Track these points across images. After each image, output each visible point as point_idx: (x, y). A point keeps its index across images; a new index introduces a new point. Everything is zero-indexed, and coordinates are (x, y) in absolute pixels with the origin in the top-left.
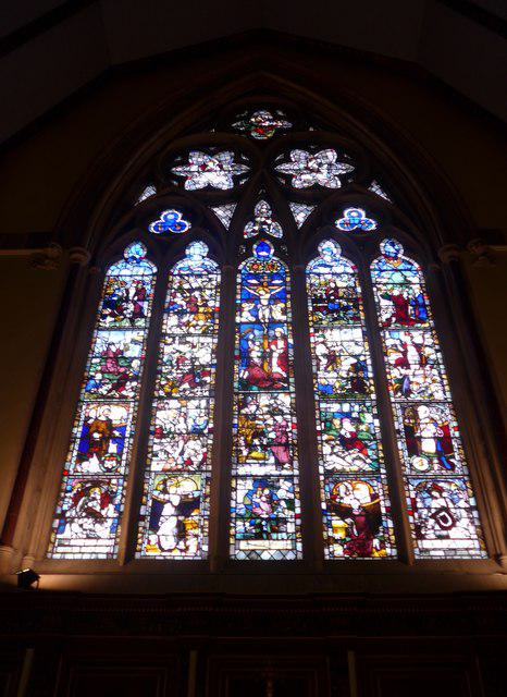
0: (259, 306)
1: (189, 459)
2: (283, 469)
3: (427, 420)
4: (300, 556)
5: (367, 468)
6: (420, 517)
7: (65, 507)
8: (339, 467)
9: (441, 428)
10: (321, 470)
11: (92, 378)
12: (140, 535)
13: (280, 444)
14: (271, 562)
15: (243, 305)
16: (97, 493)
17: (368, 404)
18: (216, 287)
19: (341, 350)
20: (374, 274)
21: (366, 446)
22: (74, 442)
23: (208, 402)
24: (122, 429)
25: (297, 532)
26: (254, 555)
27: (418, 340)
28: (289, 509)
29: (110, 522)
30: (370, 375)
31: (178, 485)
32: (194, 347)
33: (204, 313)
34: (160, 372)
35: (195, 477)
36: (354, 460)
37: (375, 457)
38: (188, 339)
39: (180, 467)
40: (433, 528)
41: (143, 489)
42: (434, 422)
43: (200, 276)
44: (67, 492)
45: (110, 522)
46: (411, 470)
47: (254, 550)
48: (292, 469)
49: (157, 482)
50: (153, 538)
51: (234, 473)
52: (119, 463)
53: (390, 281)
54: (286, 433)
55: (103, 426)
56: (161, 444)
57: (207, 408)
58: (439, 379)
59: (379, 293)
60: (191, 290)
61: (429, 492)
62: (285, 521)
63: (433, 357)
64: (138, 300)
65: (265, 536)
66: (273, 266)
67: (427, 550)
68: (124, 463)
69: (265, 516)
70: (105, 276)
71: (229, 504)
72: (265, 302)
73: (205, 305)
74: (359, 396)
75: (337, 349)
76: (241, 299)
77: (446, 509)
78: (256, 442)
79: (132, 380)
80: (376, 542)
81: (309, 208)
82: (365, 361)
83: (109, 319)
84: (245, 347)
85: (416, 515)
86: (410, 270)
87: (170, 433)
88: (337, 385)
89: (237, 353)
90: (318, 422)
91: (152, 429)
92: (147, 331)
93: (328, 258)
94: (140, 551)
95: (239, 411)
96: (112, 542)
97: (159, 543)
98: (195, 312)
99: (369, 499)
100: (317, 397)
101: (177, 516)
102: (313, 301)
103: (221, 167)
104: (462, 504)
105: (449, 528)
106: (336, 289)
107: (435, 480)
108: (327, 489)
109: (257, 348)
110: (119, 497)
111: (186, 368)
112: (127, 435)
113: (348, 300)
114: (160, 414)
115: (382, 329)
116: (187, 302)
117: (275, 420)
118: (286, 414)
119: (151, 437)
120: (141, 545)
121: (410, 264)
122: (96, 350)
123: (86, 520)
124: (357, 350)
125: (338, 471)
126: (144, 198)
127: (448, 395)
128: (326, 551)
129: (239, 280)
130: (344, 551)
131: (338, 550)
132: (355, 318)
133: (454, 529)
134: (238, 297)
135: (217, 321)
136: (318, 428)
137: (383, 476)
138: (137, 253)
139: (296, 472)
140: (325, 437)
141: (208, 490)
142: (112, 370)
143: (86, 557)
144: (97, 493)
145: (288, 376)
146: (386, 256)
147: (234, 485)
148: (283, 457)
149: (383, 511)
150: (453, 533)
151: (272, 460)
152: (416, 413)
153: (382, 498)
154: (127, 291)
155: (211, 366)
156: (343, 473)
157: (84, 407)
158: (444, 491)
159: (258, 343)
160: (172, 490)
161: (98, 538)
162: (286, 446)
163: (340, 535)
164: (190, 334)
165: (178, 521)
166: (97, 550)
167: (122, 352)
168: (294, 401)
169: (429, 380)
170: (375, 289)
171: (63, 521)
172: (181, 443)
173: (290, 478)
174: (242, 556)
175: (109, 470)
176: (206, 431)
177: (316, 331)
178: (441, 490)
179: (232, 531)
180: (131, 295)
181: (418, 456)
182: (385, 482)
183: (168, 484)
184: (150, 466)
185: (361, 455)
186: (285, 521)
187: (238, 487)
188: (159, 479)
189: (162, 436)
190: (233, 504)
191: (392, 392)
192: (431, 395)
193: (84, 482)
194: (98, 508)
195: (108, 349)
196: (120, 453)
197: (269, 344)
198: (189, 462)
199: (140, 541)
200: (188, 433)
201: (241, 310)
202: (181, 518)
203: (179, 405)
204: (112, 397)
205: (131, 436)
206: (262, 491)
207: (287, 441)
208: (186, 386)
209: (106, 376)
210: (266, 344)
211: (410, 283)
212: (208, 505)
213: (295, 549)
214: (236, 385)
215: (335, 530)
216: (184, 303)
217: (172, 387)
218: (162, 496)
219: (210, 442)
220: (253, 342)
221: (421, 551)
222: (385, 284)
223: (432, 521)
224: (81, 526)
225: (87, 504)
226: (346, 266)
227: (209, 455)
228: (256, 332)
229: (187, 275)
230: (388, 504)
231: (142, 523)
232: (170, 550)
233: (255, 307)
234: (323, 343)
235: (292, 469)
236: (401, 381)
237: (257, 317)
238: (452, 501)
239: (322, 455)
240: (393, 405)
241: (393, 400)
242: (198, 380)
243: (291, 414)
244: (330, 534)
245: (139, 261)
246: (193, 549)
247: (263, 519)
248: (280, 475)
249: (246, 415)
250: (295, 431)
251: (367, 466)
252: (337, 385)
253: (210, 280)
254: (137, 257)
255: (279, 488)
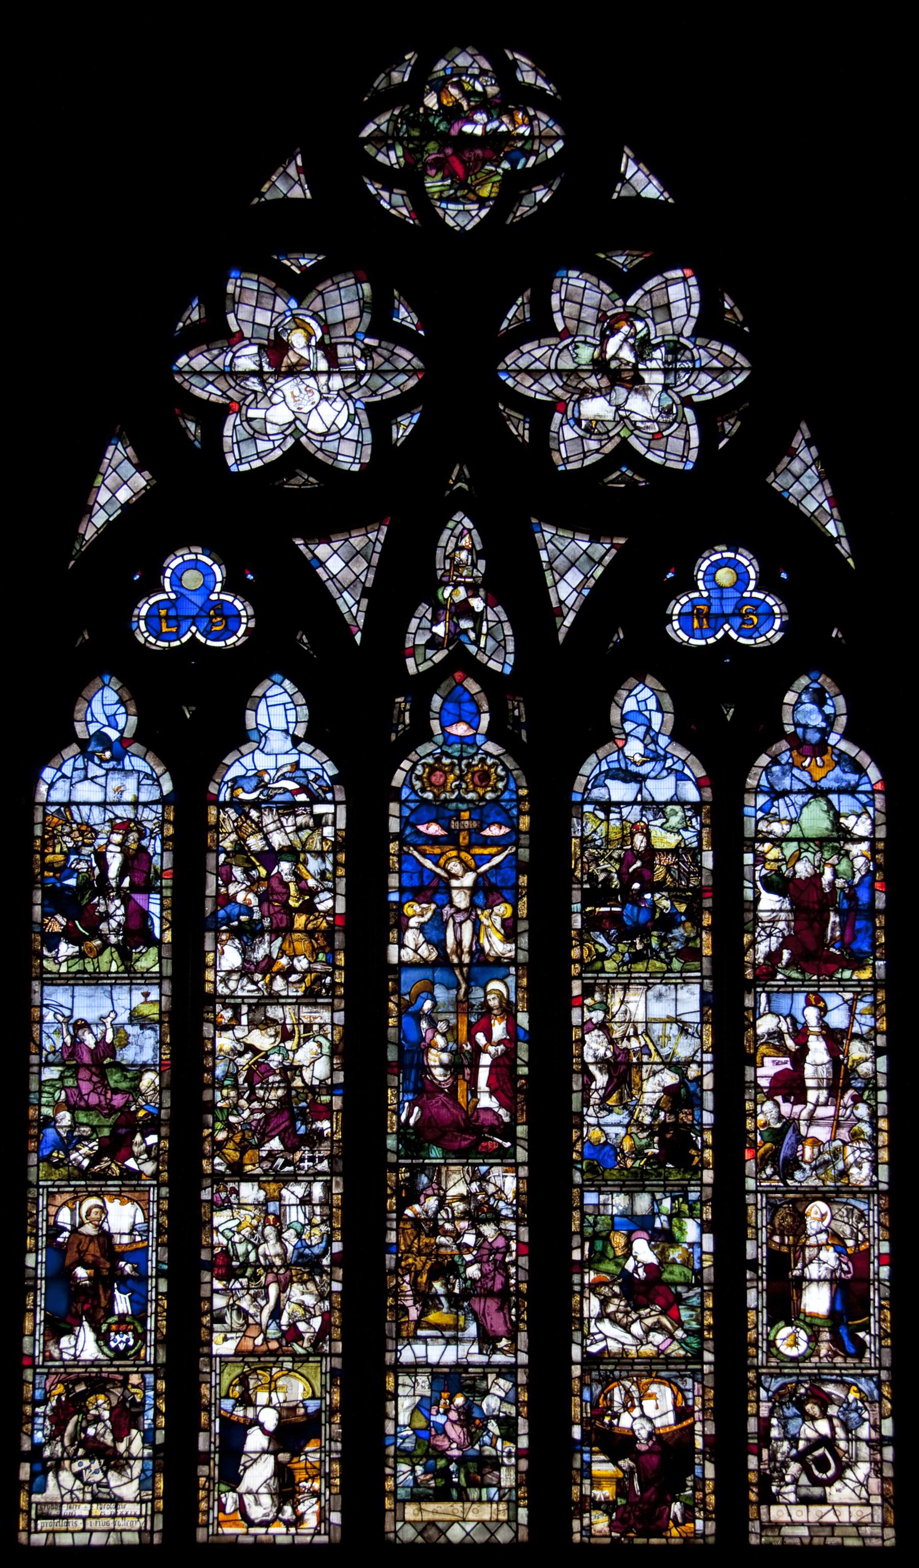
0: (447, 910)
1: (293, 1326)
2: (495, 1350)
3: (823, 1237)
4: (523, 1534)
5: (675, 1349)
6: (773, 1458)
7: (39, 1436)
8: (614, 1347)
9: (850, 1257)
10: (576, 1353)
11: (49, 1122)
12: (202, 1494)
13: (489, 1294)
14: (466, 1548)
15: (408, 910)
16: (101, 1405)
17: (693, 1196)
18: (336, 848)
19: (644, 1050)
20: (755, 803)
21: (679, 1300)
22: (35, 1289)
23: (327, 1188)
24: (137, 1254)
25: (518, 1486)
26: (432, 1532)
27: (837, 1019)
28: (505, 1437)
29: (137, 1467)
30: (708, 1118)
31: (272, 1387)
32: (287, 1036)
33: (310, 934)
34: (212, 1107)
35: (310, 1369)
36: (648, 1331)
37: (694, 1325)
38: (275, 1012)
39: (274, 1345)
40: (795, 1481)
41: (200, 1396)
42: (836, 1240)
43: (290, 808)
44: (36, 1403)
45: (137, 1467)
46: (769, 1354)
47: (432, 1523)
48: (515, 1352)
49: (226, 1380)
50: (230, 1501)
51: (389, 1358)
52: (140, 1337)
53: (795, 831)
54: (505, 1266)
55: (94, 1249)
56: (226, 1291)
57: (326, 1203)
58: (866, 1129)
59: (761, 872)
60: (271, 857)
61: (800, 1405)
62: (495, 1464)
63: (865, 1068)
64: (133, 887)
65: (454, 1493)
66: (485, 777)
67: (778, 1526)
68: (151, 1337)
69: (456, 1453)
70: (31, 804)
71: (382, 1427)
72: (461, 900)
73: (309, 908)
74: (675, 1177)
75: (634, 1044)
76: (401, 890)
77: (828, 1442)
78: (438, 1286)
79: (146, 1129)
80: (676, 1508)
81: (598, 550)
82: (699, 1079)
83: (65, 949)
84: (413, 1036)
85: (765, 1453)
86: (851, 791)
87: (245, 1264)
88: (627, 1145)
89: (392, 1054)
90: (576, 1241)
91: (205, 1255)
92: (167, 987)
93: (634, 748)
94: (206, 1525)
95: (400, 1211)
96: (147, 1509)
97: (241, 1508)
98: (283, 930)
99: (670, 1418)
100: (577, 1178)
101: (275, 1453)
102: (592, 897)
103: (329, 350)
104: (864, 1431)
105: (830, 1482)
106: (651, 852)
107: (817, 1379)
108: (586, 1395)
109: (440, 1041)
110: (150, 1414)
111: (273, 1095)
112: (151, 1272)
113: (675, 895)
114: (220, 1219)
115: (750, 986)
116: (263, 899)
117: (479, 1235)
118: (506, 1218)
119: (206, 1276)
120: (207, 1512)
121: (859, 770)
122: (47, 1044)
123: (86, 1463)
124: (684, 1048)
125: (612, 1356)
126: (90, 533)
127: (884, 1173)
128: (576, 1524)
129: (394, 826)
130: (611, 1525)
131: (600, 1523)
132: (690, 953)
133: (838, 1485)
134: (393, 881)
135: (341, 959)
136: (576, 1255)
137: (707, 1369)
138: (112, 721)
139: (523, 1358)
140: (590, 1277)
141: (337, 1397)
142: (94, 1099)
143: (98, 1539)
144: (101, 1405)
145: (514, 1123)
146: (797, 743)
147: (390, 1387)
148: (497, 1323)
149: (699, 1443)
150: (836, 1493)
151: (472, 1330)
152: (800, 1218)
153: (698, 1416)
154: (101, 857)
155: (331, 1089)
156: (622, 1359)
157: (42, 1201)
158: (832, 1402)
159: (442, 1026)
160: (262, 1397)
161: (117, 1501)
162: (503, 1296)
163: (605, 1492)
164: (274, 999)
165: (277, 1463)
166: (121, 1524)
167: (111, 1050)
168: (523, 1187)
169: (844, 1134)
170: (748, 858)
171: (38, 1467)
172: (273, 1290)
173: (506, 1372)
174: (408, 1534)
175: (120, 1354)
176: (326, 1261)
177: (588, 991)
178: (825, 1401)
179: (389, 1484)
180: (113, 872)
181: (789, 1324)
182: (709, 1381)
183: (252, 1383)
184: (209, 1343)
185: (665, 1321)
186: (495, 1464)
187: (401, 1391)
188: (231, 1373)
189: (230, 1274)
190: (390, 1428)
191: (750, 1166)
192: (844, 1173)
193: (70, 1382)
194: (109, 1439)
195: (77, 1042)
196: (139, 1315)
197: (472, 1030)
198: (293, 1334)
199: (203, 1505)
200: (286, 1265)
201: (403, 928)
202: (284, 1457)
203: (261, 1195)
204: (104, 1176)
205: (160, 1274)
206: (451, 1399)
207: (506, 1285)
208: (275, 1144)
209: (82, 1117)
210: (463, 1029)
211: (846, 835)
212: (337, 1429)
213: (512, 1520)
214: (391, 1142)
215: (596, 1482)
216: (254, 900)
217: (243, 1148)
218: (239, 1412)
219: (337, 1287)
220: (433, 1024)
221: (763, 1527)
222: (778, 842)
223: (794, 1468)
224: (78, 1476)
225: (84, 1430)
226: (681, 777)
227: (336, 1318)
228: (440, 993)
229: (256, 804)
230: (710, 1429)
231: (203, 1470)
232: (266, 1524)
233: (437, 914)
234: (603, 1026)
235: (515, 1352)
236: (777, 1136)
237: (440, 945)
238: (845, 1425)
239: (581, 1319)
240: (750, 1199)
241: (750, 1184)
242: (302, 1130)
243: (517, 1220)
244: (586, 1490)
245: (120, 750)
246: (311, 1521)
247: (450, 1460)
248: (489, 1365)
249: (416, 1222)
250: (524, 1261)
251: (675, 1346)
252: (627, 1145)
253: (319, 822)
254: (114, 735)
255: (486, 1393)
